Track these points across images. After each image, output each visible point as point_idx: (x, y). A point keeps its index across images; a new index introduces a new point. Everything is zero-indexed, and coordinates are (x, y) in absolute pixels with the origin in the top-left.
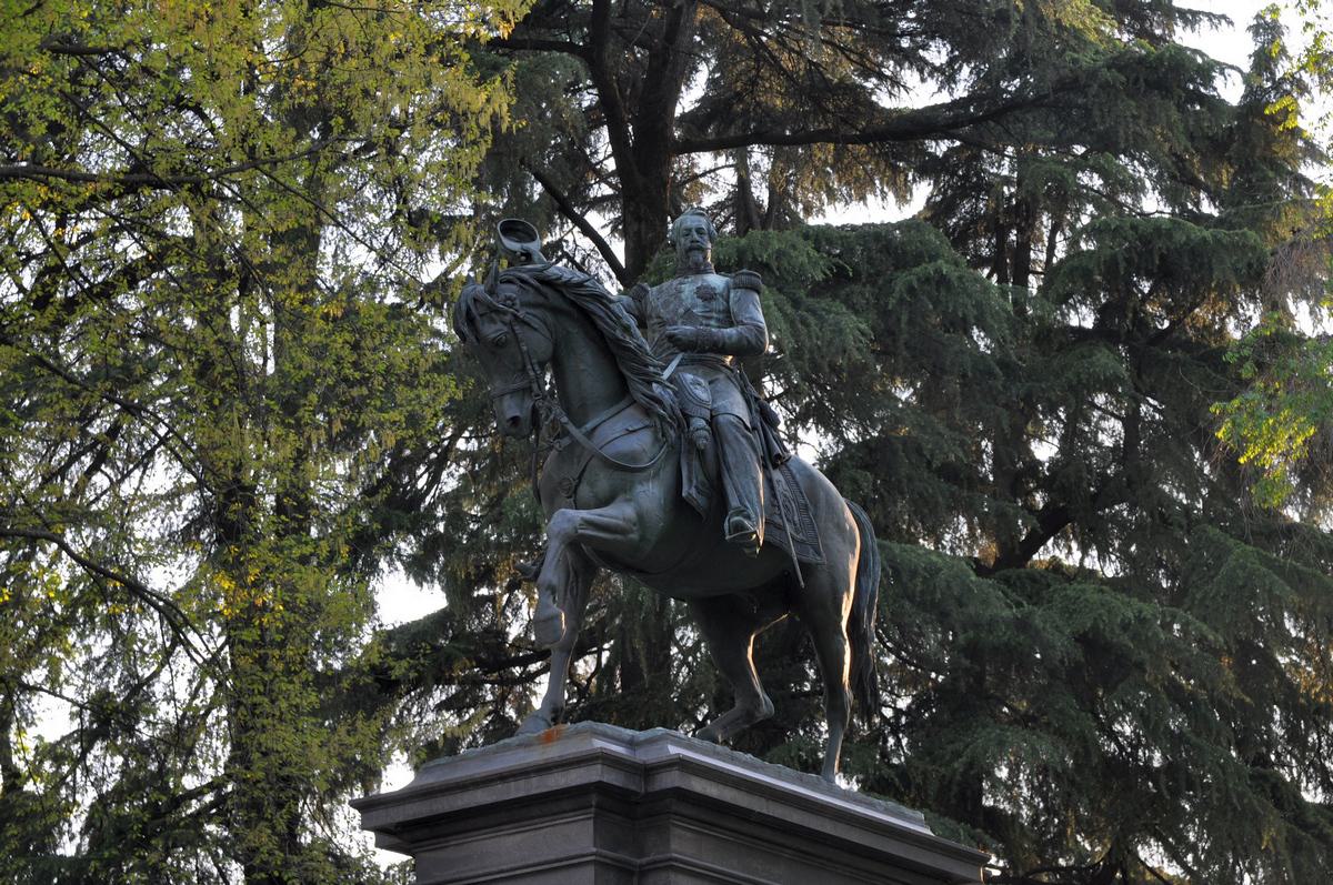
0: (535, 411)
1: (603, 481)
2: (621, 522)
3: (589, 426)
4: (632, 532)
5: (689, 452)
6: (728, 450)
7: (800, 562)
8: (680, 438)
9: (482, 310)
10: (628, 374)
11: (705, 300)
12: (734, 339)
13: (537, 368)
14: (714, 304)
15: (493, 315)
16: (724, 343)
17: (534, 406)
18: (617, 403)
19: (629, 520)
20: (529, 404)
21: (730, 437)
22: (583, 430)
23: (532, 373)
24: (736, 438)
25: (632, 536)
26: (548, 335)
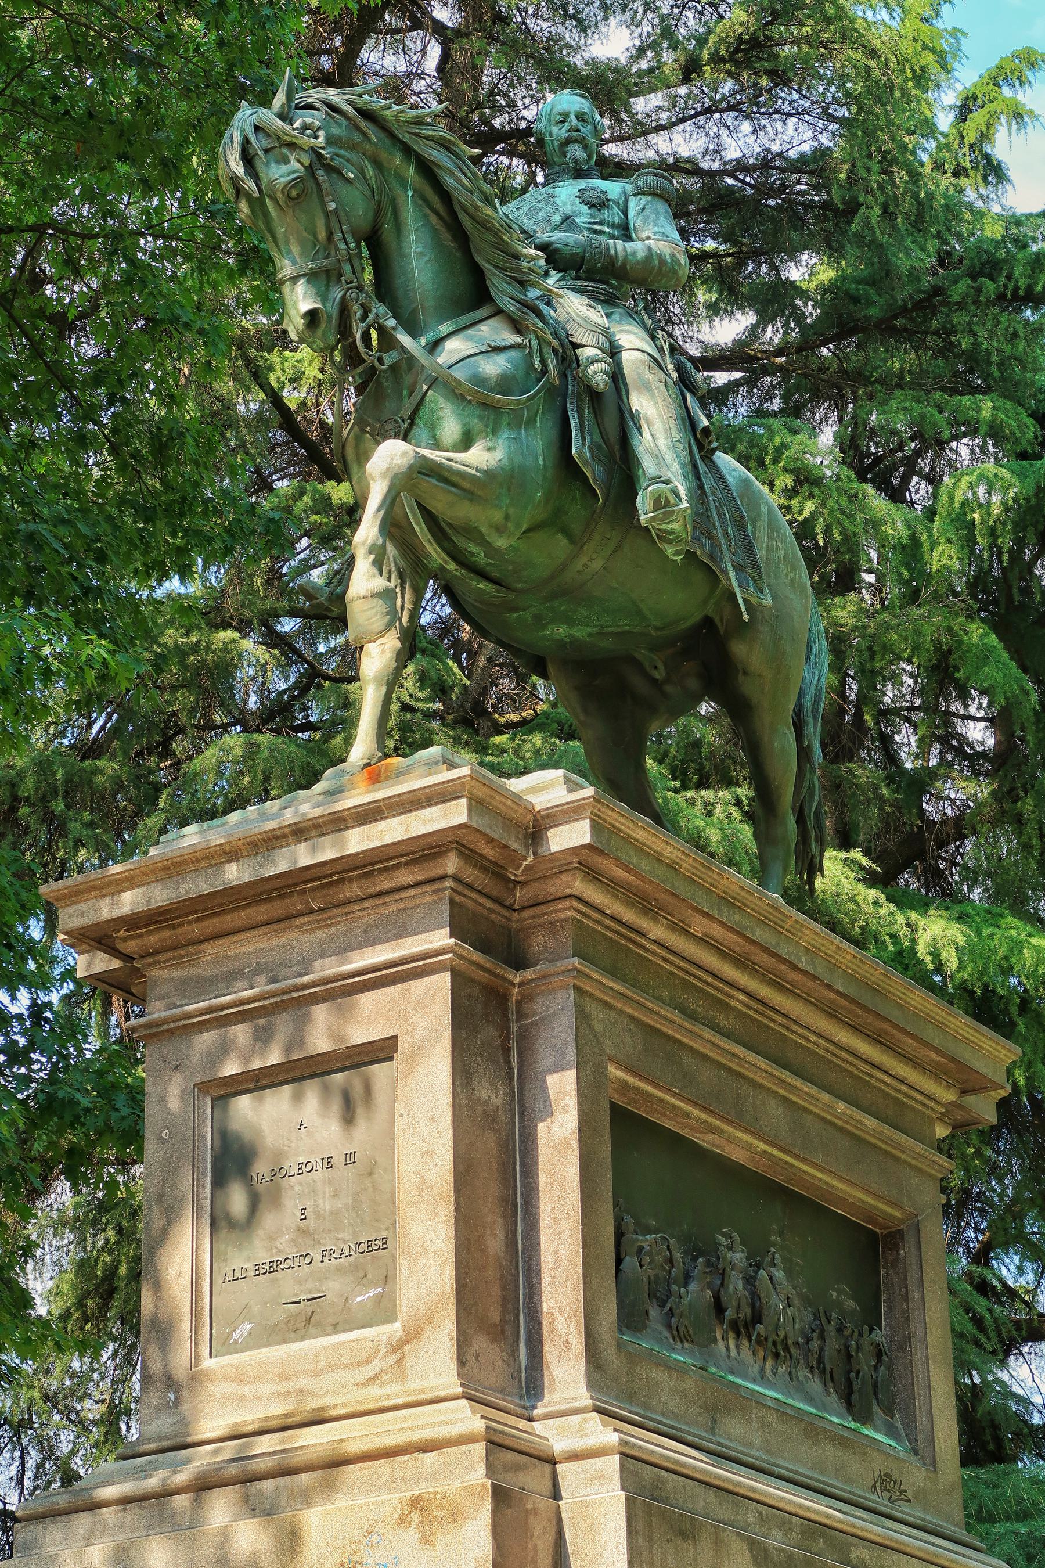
5: (580, 400)
9: (266, 143)
10: (486, 266)
11: (592, 206)
12: (641, 254)
13: (350, 239)
14: (606, 215)
15: (285, 150)
16: (624, 265)
17: (344, 297)
20: (337, 293)
22: (423, 340)
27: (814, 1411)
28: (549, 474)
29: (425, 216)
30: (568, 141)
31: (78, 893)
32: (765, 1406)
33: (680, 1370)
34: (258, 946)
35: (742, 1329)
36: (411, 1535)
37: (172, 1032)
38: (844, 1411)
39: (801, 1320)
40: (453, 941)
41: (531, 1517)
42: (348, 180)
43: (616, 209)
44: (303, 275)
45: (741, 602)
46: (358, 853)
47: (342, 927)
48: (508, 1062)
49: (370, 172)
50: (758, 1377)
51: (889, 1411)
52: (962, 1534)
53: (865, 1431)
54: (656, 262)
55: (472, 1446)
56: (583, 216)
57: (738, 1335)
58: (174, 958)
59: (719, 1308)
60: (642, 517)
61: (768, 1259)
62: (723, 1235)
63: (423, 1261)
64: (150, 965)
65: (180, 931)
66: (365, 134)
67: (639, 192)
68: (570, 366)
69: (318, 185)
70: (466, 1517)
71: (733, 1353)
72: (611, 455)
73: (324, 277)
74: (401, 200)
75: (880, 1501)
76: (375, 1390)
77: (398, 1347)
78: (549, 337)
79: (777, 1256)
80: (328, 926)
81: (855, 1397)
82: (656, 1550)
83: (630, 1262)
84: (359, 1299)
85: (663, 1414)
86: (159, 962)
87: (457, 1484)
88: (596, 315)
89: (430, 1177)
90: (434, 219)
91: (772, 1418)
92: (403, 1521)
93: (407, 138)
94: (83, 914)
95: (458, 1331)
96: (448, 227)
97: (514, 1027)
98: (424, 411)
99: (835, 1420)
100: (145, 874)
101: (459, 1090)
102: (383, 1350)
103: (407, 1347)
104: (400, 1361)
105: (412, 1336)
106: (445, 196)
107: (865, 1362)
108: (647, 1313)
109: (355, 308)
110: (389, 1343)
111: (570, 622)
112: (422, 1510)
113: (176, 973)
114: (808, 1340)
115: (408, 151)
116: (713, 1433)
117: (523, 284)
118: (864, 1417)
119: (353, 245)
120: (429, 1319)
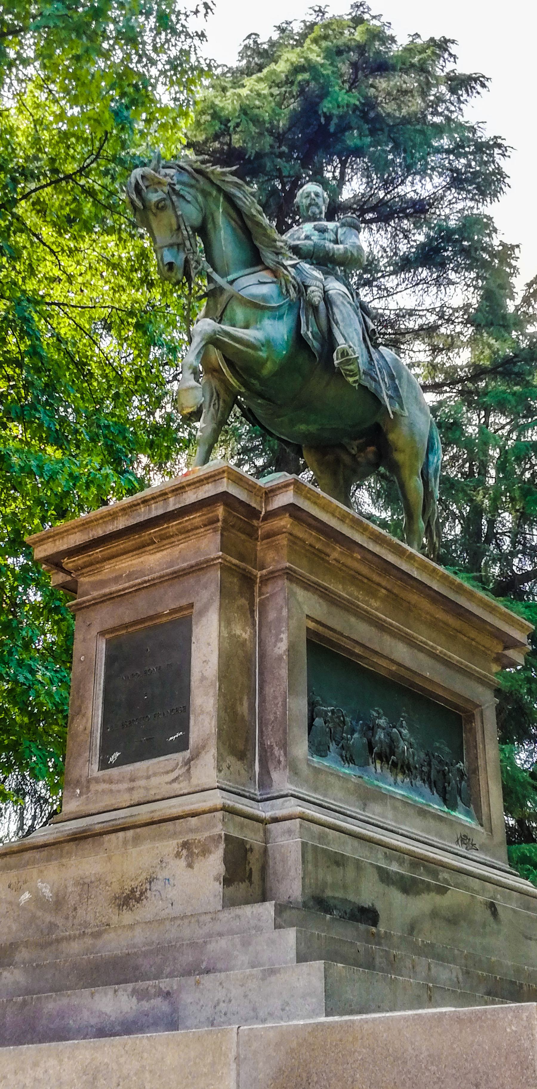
0: (187, 261)
1: (240, 313)
2: (252, 340)
3: (230, 278)
4: (261, 350)
5: (307, 310)
6: (335, 310)
7: (393, 412)
8: (300, 299)
9: (147, 183)
12: (342, 251)
13: (189, 229)
14: (326, 235)
16: (333, 255)
18: (247, 267)
19: (258, 340)
21: (338, 303)
23: (185, 232)
24: (343, 303)
25: (261, 353)
26: (198, 207)
27: (424, 802)
28: (291, 342)
29: (229, 222)
30: (310, 205)
31: (42, 540)
32: (394, 798)
33: (345, 779)
34: (130, 563)
35: (383, 757)
36: (182, 863)
37: (87, 607)
38: (442, 803)
39: (418, 756)
40: (221, 553)
41: (249, 853)
42: (189, 202)
43: (331, 233)
44: (166, 246)
45: (390, 412)
46: (173, 511)
47: (169, 550)
48: (253, 617)
49: (200, 198)
50: (393, 783)
51: (467, 804)
52: (507, 867)
53: (453, 813)
54: (350, 254)
55: (215, 813)
56: (316, 237)
57: (382, 761)
58: (90, 571)
59: (370, 747)
60: (336, 362)
61: (399, 723)
62: (375, 711)
63: (201, 717)
64: (79, 575)
65: (92, 557)
66: (197, 181)
67: (343, 225)
68: (302, 295)
69: (173, 203)
70: (210, 852)
71: (379, 770)
72: (323, 337)
73: (176, 247)
74: (216, 214)
75: (461, 850)
76: (175, 785)
77: (188, 763)
78: (290, 279)
79: (404, 722)
80: (162, 550)
81: (448, 796)
82: (320, 871)
83: (318, 721)
84: (171, 738)
85: (334, 800)
86: (83, 574)
87: (207, 834)
88: (318, 274)
89: (206, 674)
90: (233, 223)
91: (398, 804)
92: (178, 855)
93: (218, 183)
94: (45, 550)
95: (218, 753)
96: (241, 228)
97: (257, 600)
98: (228, 312)
99: (436, 807)
100: (73, 528)
101: (223, 629)
102: (180, 764)
103: (192, 762)
104: (188, 770)
105: (195, 756)
106: (238, 211)
107: (454, 778)
108: (329, 747)
109: (192, 262)
110: (183, 761)
111: (307, 422)
112: (188, 849)
113: (92, 579)
114: (422, 766)
115: (219, 189)
116: (364, 811)
117: (277, 254)
118: (453, 807)
119: (191, 233)
120: (204, 747)
